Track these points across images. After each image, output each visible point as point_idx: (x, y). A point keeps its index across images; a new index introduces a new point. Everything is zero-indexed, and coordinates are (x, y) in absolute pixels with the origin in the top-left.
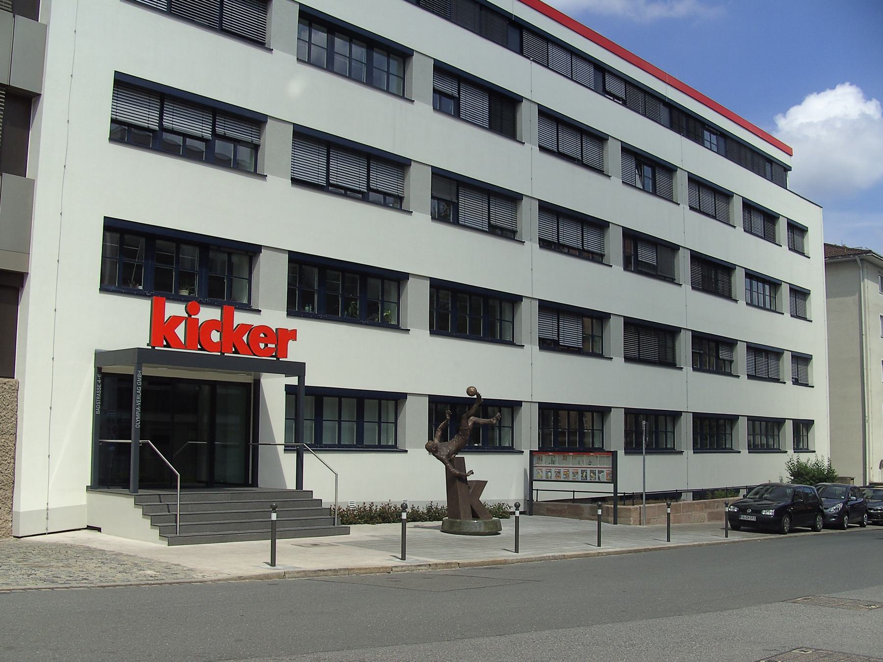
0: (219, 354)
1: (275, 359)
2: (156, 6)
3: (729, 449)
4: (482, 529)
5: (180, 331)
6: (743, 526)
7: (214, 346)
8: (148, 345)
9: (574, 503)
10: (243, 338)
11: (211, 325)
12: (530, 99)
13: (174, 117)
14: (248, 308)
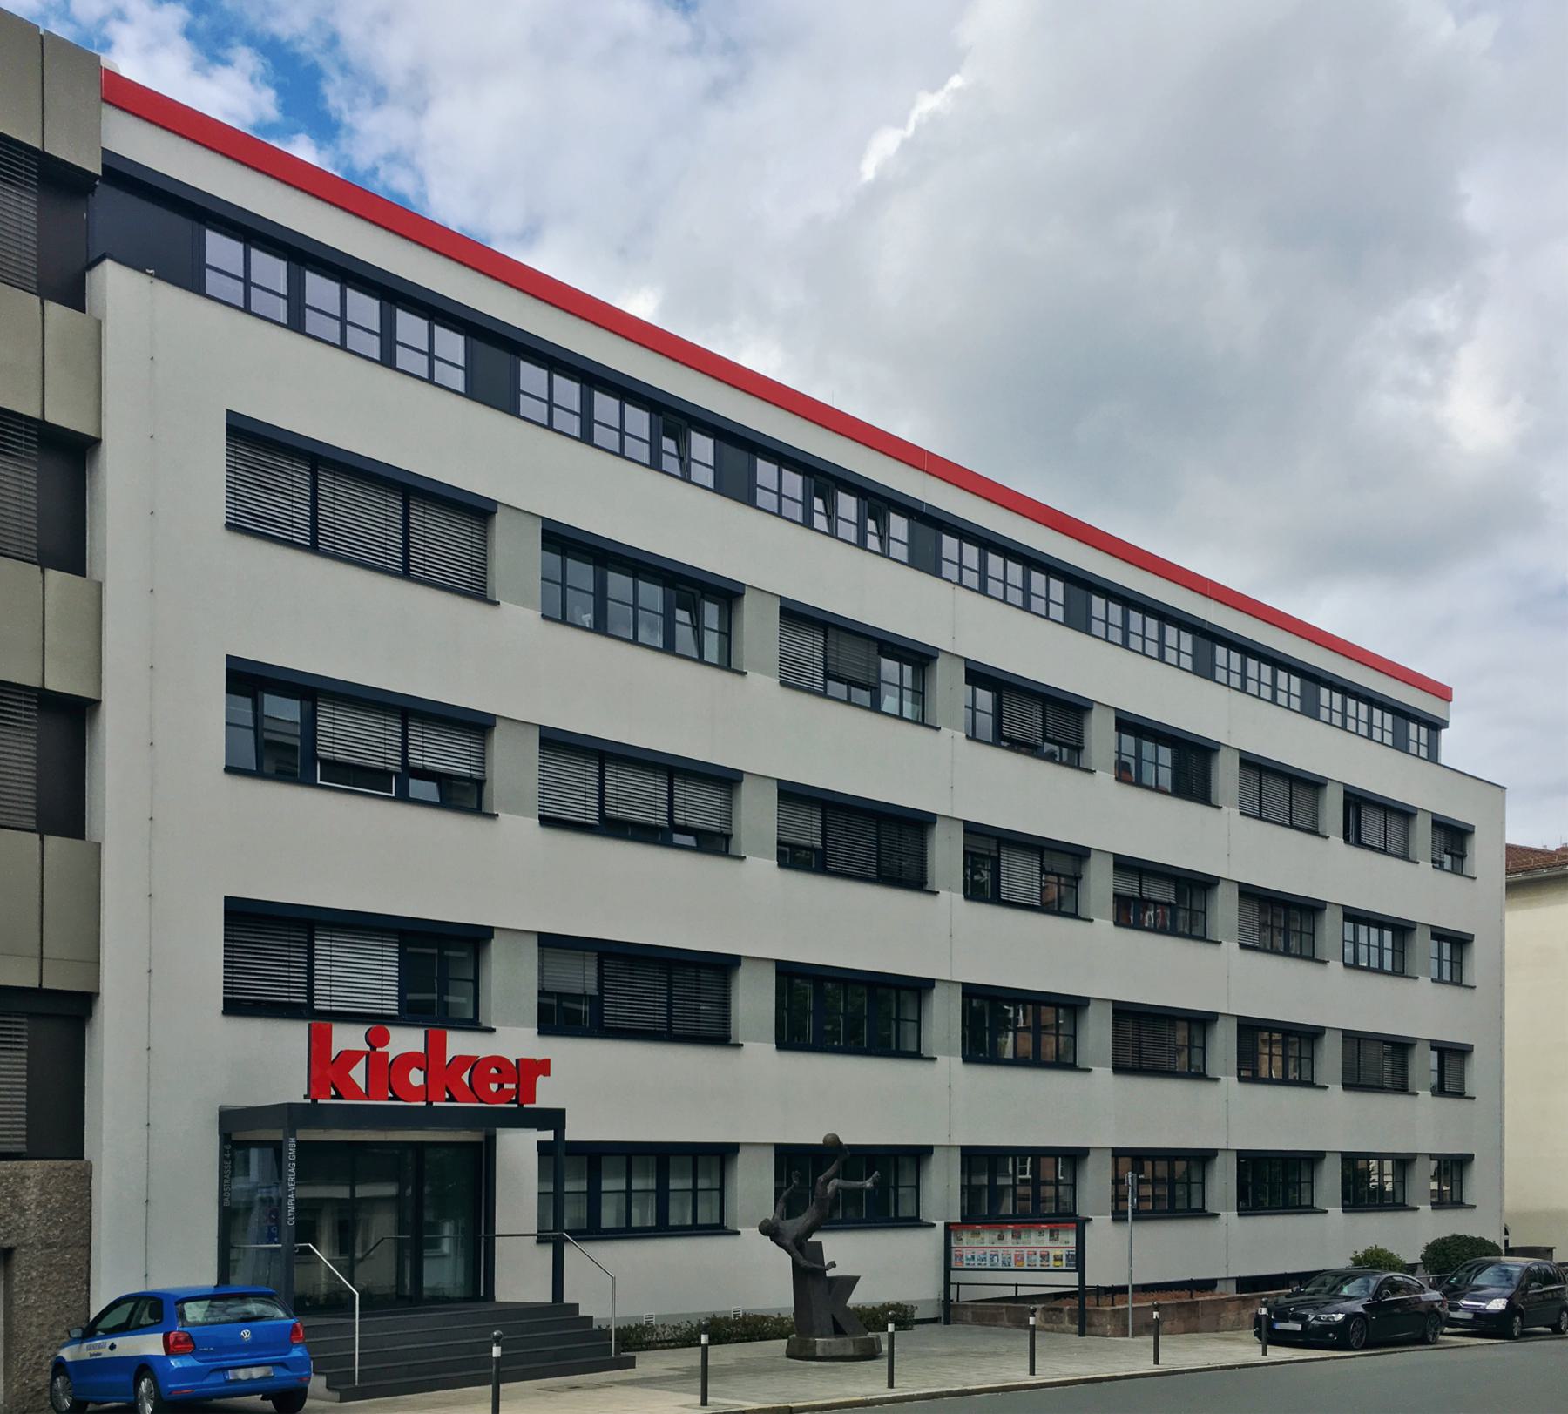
0: (424, 1104)
1: (516, 1106)
2: (290, 538)
3: (1307, 1207)
4: (850, 1351)
5: (358, 1074)
6: (1449, 1327)
7: (414, 1093)
8: (305, 1097)
9: (1016, 1303)
10: (463, 1077)
11: (408, 1060)
12: (951, 651)
13: (335, 727)
14: (473, 1024)
